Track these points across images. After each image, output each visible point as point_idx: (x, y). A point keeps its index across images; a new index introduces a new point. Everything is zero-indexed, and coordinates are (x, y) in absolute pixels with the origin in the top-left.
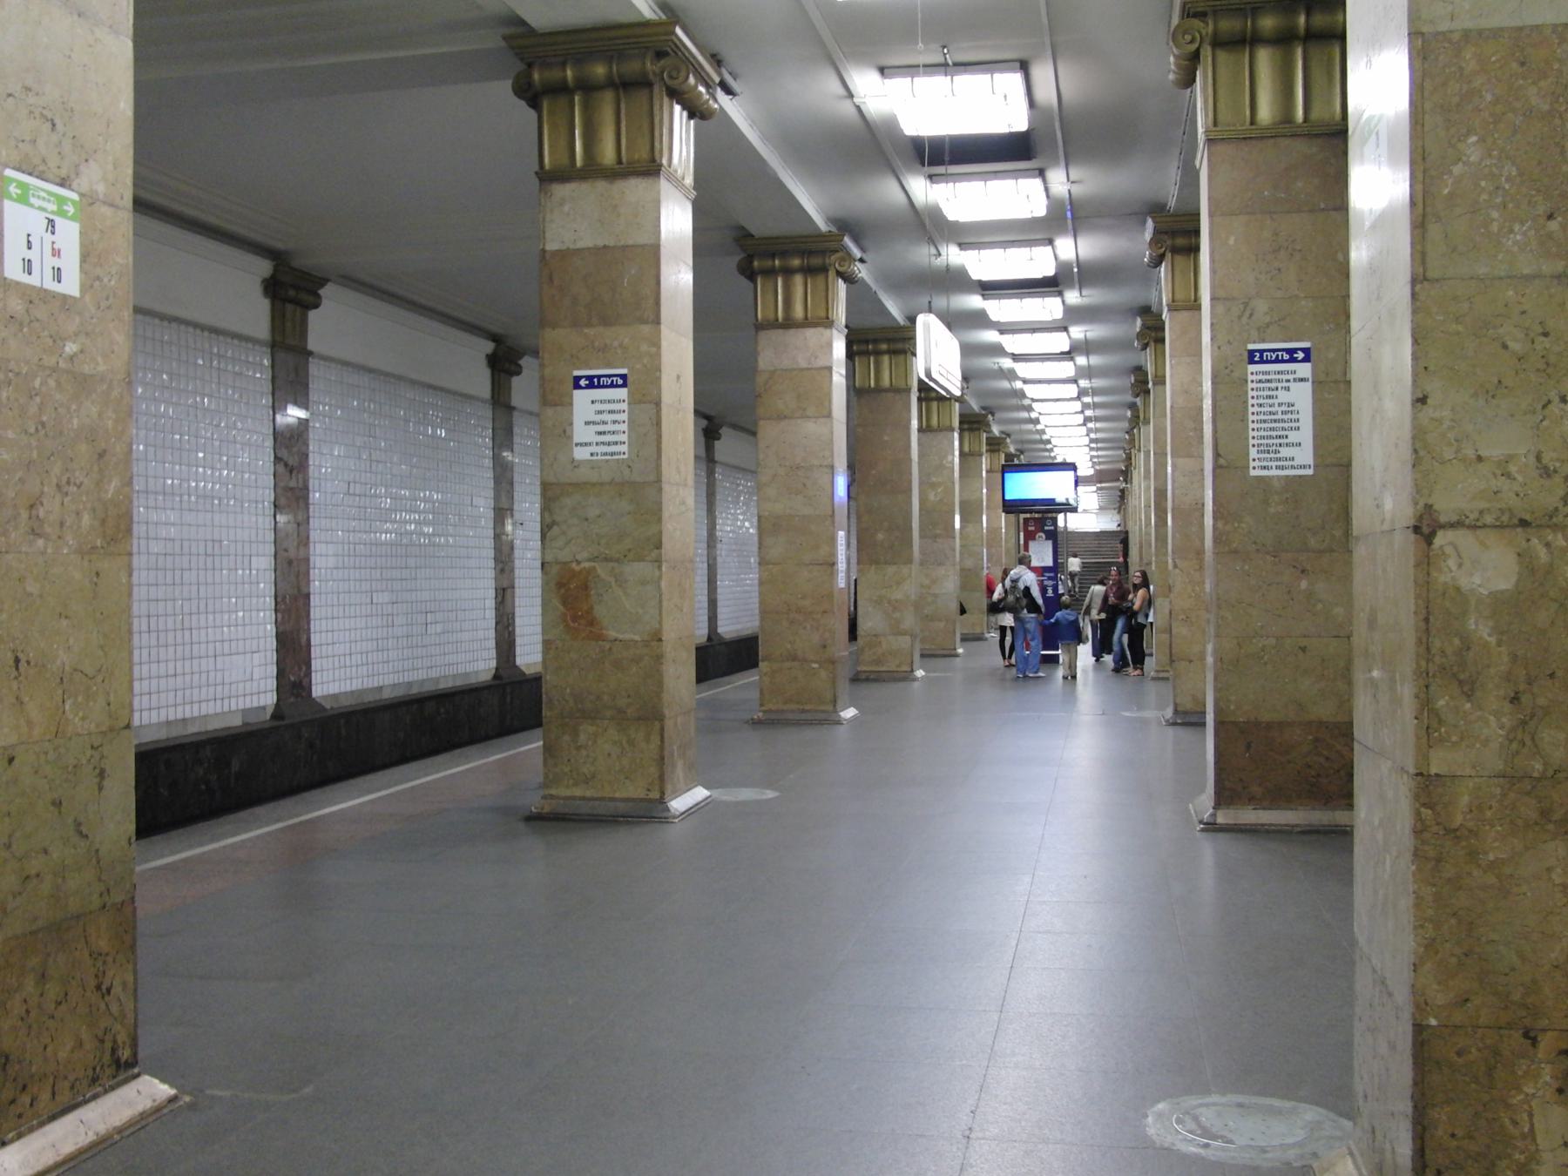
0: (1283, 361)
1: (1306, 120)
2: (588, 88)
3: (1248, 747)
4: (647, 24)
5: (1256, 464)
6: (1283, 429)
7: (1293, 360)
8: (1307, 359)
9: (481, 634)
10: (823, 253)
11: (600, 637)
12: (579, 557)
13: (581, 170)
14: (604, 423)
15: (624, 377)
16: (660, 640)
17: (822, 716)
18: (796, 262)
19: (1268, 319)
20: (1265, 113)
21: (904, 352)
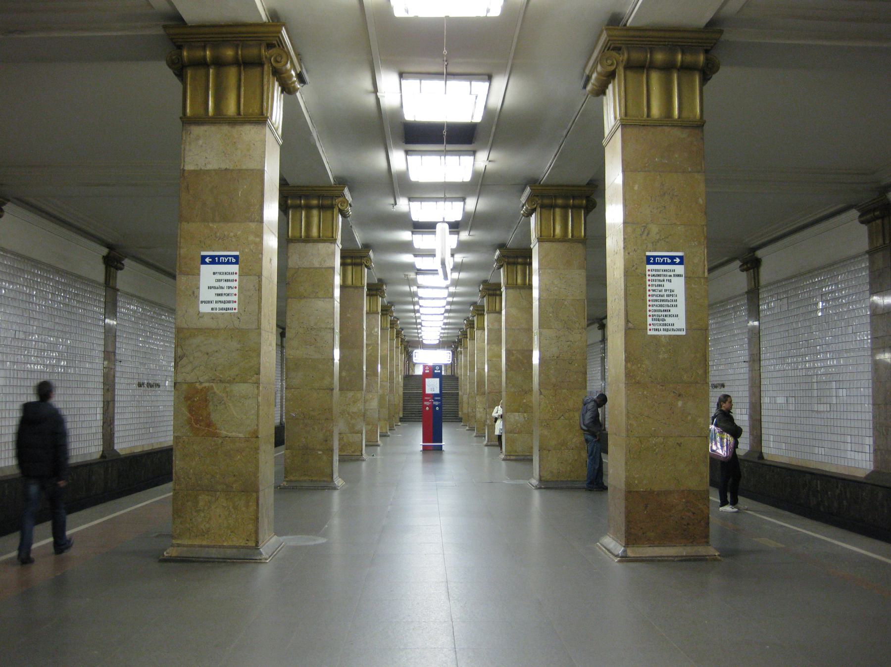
0: (667, 264)
1: (679, 117)
2: (219, 64)
3: (646, 506)
4: (263, 25)
5: (652, 327)
6: (668, 306)
7: (673, 263)
8: (681, 263)
9: (94, 430)
10: (332, 197)
11: (215, 435)
12: (201, 379)
13: (212, 118)
14: (222, 288)
15: (236, 257)
16: (257, 437)
17: (325, 484)
18: (315, 202)
19: (658, 237)
20: (656, 111)
21: (495, 295)
